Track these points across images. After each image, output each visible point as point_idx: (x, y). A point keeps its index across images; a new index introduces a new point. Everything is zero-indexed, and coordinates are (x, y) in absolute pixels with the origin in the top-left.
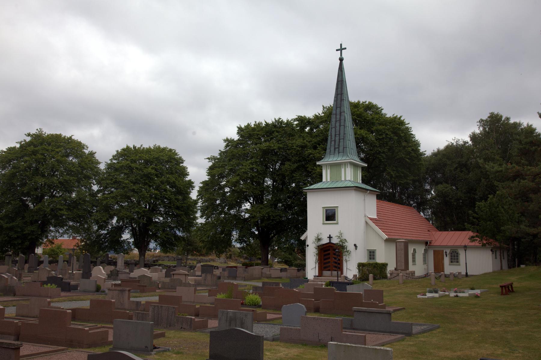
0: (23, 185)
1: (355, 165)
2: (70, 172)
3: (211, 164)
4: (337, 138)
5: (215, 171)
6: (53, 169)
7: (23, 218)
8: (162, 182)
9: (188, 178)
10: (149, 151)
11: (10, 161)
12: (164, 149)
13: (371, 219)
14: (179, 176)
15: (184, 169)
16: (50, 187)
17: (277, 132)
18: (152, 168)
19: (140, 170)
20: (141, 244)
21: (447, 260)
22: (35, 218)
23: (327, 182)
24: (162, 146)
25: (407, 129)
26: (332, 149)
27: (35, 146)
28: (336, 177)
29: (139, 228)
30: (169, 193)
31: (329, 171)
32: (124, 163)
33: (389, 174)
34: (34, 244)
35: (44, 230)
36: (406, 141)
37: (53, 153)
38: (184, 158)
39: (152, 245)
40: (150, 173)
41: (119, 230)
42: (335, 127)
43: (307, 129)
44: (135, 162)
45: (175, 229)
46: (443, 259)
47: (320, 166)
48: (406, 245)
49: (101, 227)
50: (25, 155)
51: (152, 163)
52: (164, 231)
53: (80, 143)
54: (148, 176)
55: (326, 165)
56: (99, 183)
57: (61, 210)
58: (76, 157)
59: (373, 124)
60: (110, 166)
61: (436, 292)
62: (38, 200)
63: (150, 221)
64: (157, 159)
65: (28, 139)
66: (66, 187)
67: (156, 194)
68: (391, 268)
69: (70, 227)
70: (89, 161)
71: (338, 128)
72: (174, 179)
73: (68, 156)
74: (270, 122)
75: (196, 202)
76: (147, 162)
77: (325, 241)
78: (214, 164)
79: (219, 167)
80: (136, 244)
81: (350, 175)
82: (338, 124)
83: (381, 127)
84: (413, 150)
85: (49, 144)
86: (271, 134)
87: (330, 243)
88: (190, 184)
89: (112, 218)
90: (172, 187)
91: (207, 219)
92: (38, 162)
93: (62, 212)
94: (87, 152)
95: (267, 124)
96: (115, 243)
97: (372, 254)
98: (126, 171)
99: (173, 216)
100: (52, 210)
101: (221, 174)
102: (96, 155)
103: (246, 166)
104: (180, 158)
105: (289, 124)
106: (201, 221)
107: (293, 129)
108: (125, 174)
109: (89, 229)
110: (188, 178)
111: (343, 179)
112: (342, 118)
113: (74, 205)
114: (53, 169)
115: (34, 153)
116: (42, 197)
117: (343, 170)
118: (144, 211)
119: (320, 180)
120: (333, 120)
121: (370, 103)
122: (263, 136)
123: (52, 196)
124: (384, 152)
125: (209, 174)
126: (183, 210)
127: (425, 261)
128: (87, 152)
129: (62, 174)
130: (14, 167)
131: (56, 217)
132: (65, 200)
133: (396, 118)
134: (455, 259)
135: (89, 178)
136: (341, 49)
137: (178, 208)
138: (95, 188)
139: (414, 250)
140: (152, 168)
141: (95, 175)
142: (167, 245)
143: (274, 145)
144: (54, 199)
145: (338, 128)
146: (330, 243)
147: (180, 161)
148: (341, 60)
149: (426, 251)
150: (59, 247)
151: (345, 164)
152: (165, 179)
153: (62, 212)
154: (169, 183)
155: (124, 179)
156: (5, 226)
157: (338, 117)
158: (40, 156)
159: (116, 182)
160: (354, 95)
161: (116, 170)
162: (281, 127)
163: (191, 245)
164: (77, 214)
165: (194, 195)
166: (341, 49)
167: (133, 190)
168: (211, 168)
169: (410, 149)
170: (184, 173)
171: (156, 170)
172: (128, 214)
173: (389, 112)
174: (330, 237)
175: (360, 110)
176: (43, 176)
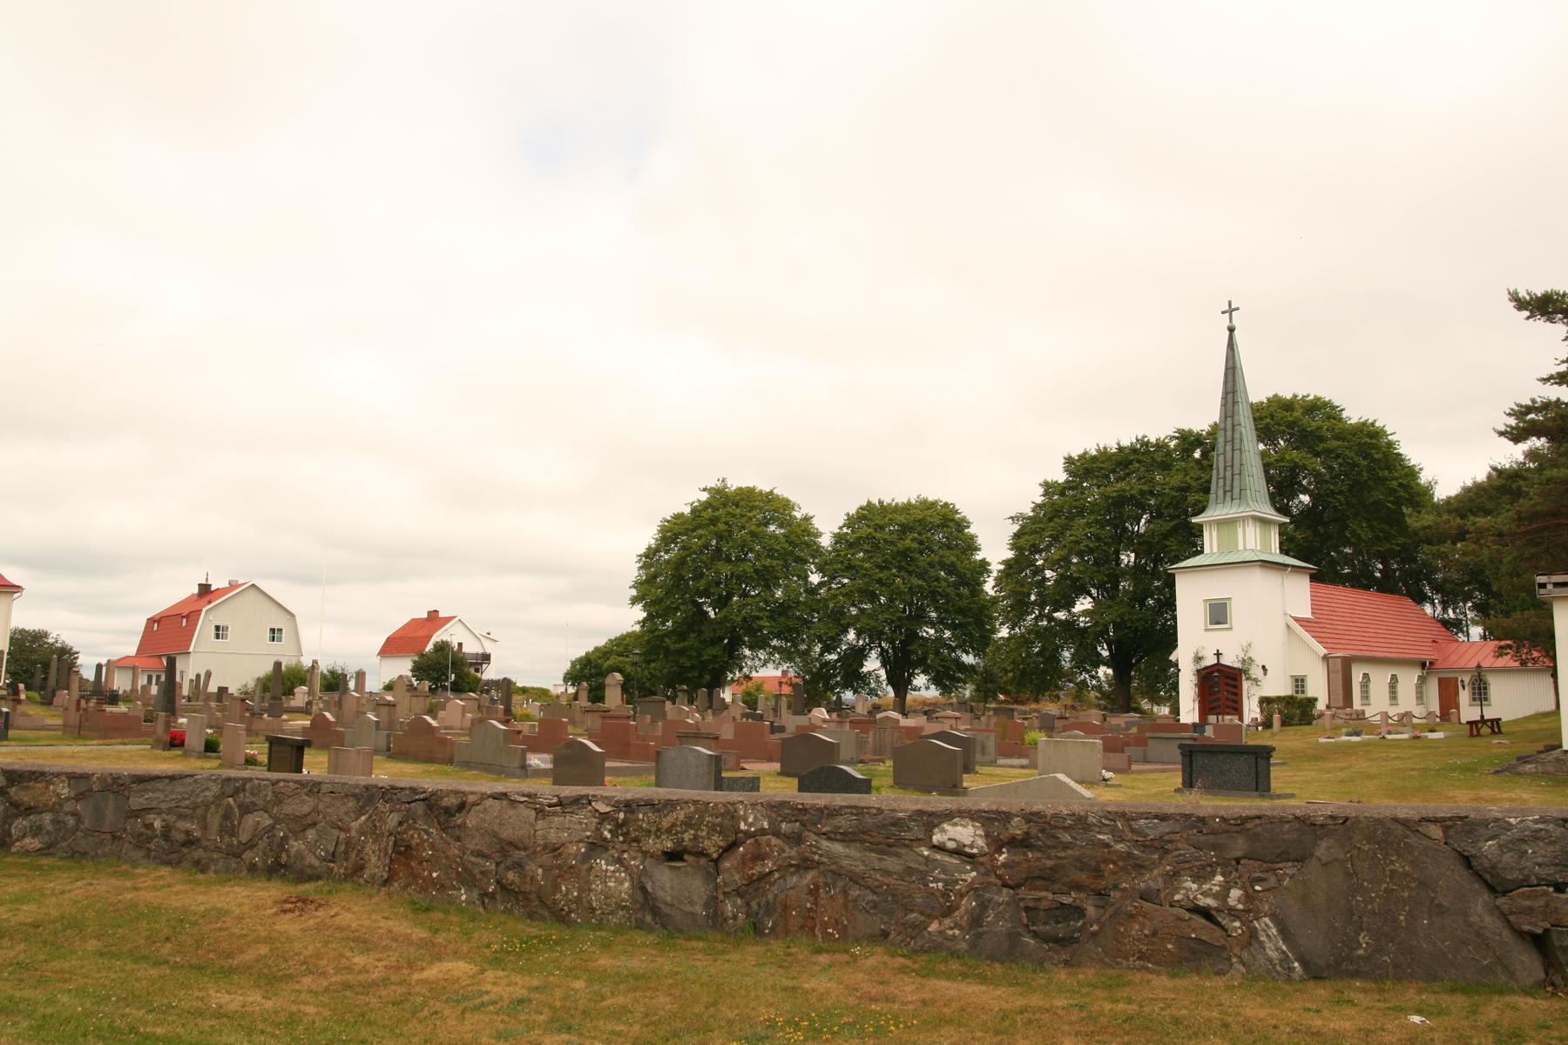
0: (698, 576)
1: (1264, 522)
2: (771, 553)
3: (1016, 528)
4: (1229, 474)
5: (1022, 541)
6: (744, 547)
7: (700, 633)
8: (931, 565)
9: (979, 557)
10: (907, 507)
11: (676, 536)
12: (934, 504)
13: (1296, 619)
14: (964, 553)
15: (972, 538)
16: (741, 578)
17: (1139, 461)
18: (913, 540)
19: (893, 543)
20: (900, 682)
21: (1464, 696)
22: (719, 633)
23: (1212, 553)
24: (931, 499)
25: (1390, 444)
26: (1221, 492)
27: (715, 509)
28: (1228, 544)
29: (894, 648)
30: (944, 584)
31: (1215, 534)
32: (865, 531)
33: (1353, 532)
34: (718, 682)
35: (732, 659)
36: (1388, 468)
37: (743, 520)
38: (970, 518)
39: (920, 680)
40: (909, 549)
41: (859, 655)
42: (1225, 453)
43: (1197, 455)
44: (882, 528)
45: (959, 652)
46: (1457, 694)
47: (1200, 527)
48: (1347, 663)
49: (828, 649)
50: (699, 526)
51: (911, 529)
52: (937, 653)
53: (788, 501)
54: (905, 554)
55: (1210, 523)
56: (820, 569)
57: (759, 618)
58: (781, 526)
59: (1322, 439)
60: (839, 538)
61: (1357, 734)
62: (722, 603)
63: (913, 636)
64: (921, 522)
65: (704, 496)
66: (766, 579)
67: (920, 587)
68: (1321, 706)
69: (775, 648)
70: (801, 534)
71: (1229, 456)
72: (953, 559)
73: (766, 524)
74: (1126, 443)
75: (995, 601)
76: (905, 529)
77: (1210, 660)
78: (1023, 527)
79: (1032, 535)
80: (890, 681)
81: (1259, 541)
82: (1229, 448)
83: (1335, 443)
84: (1401, 485)
85: (737, 506)
86: (1126, 467)
87: (1218, 664)
88: (984, 566)
89: (846, 631)
90: (950, 573)
91: (1013, 628)
92: (720, 537)
93: (761, 623)
94: (798, 515)
95: (1120, 449)
96: (853, 676)
97: (1299, 682)
98: (866, 547)
99: (953, 627)
100: (745, 619)
101: (1033, 545)
102: (814, 521)
103: (1080, 528)
104: (964, 519)
105: (1160, 446)
106: (1004, 632)
107: (1169, 453)
108: (866, 551)
109: (807, 652)
110: (979, 557)
111: (1241, 547)
112: (1237, 435)
113: (783, 609)
114: (744, 547)
115: (713, 521)
116: (730, 596)
117: (1240, 530)
118: (900, 619)
119: (1202, 552)
120: (1221, 440)
121: (1318, 399)
122: (1114, 471)
123: (745, 595)
124: (1341, 492)
125: (1014, 547)
126: (972, 620)
127: (1420, 697)
128: (798, 515)
129: (758, 555)
130: (683, 548)
131: (752, 631)
132: (766, 602)
133: (1364, 424)
134: (1480, 693)
135: (805, 562)
136: (1231, 311)
137: (961, 611)
138: (815, 579)
139: (1366, 676)
140: (913, 540)
141: (814, 557)
142: (946, 677)
143: (1132, 485)
144: (749, 600)
145: (1229, 456)
146: (1218, 664)
147: (961, 525)
148: (1231, 330)
149: (1422, 679)
150: (759, 688)
151: (1244, 519)
152: (937, 559)
153: (761, 623)
154: (943, 566)
155: (863, 560)
156: (673, 647)
157: (1229, 433)
158: (721, 526)
159: (850, 567)
160: (1258, 390)
161: (851, 545)
162: (1147, 452)
163: (992, 681)
164: (785, 627)
165: (989, 587)
166: (1231, 311)
167: (880, 581)
168: (1017, 536)
169: (1395, 483)
170: (971, 546)
171: (921, 543)
172: (872, 623)
173: (1353, 414)
174: (1218, 654)
175: (1295, 414)
176: (728, 560)
